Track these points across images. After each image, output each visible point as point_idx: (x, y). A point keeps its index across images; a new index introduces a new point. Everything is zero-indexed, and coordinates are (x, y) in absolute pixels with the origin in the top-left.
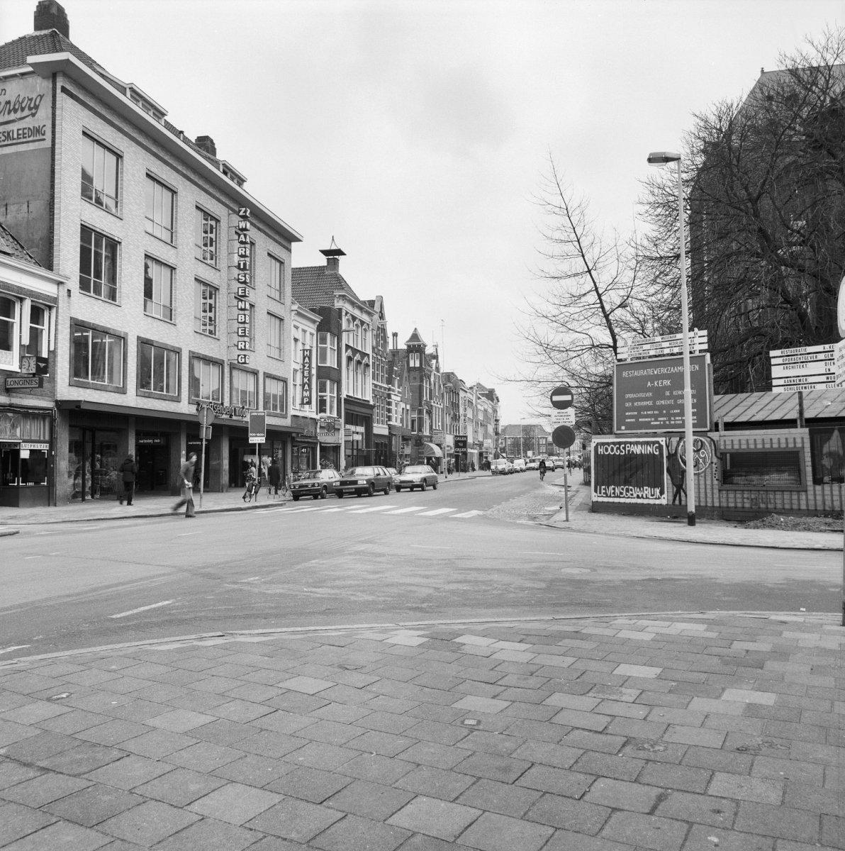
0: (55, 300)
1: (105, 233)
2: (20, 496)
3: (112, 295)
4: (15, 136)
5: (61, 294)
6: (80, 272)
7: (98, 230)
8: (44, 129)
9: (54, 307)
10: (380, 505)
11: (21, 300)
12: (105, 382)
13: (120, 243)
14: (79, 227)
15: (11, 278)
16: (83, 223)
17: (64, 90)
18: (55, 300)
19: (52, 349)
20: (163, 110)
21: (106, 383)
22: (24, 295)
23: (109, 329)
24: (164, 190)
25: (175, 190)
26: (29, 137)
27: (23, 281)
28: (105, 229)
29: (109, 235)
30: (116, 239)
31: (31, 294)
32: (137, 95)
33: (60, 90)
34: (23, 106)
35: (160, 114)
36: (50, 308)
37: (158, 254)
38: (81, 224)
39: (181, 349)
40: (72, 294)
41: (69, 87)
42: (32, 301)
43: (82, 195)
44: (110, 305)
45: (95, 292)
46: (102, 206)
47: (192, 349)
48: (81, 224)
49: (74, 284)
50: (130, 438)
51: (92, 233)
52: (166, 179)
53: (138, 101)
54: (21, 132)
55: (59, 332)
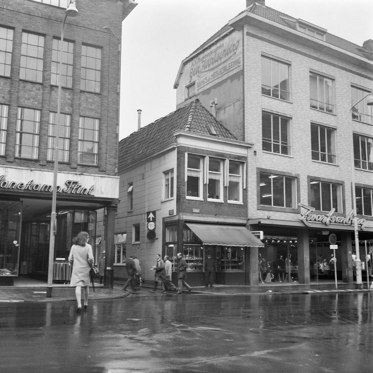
0: (246, 158)
1: (280, 114)
2: (353, 277)
3: (285, 150)
4: (228, 68)
5: (249, 154)
6: (312, 149)
7: (275, 113)
8: (240, 59)
9: (245, 162)
10: (205, 327)
11: (224, 160)
12: (197, 195)
13: (291, 118)
14: (352, 134)
15: (186, 143)
16: (263, 110)
17: (248, 34)
18: (246, 158)
19: (245, 188)
20: (324, 30)
21: (221, 200)
22: (205, 155)
23: (285, 172)
24: (272, 61)
25: (334, 78)
26: (234, 66)
27: (210, 147)
28: (358, 131)
29: (283, 115)
30: (289, 116)
31: (230, 156)
32: (304, 25)
33: (246, 35)
34: (231, 50)
35: (322, 32)
36: (243, 163)
37: (321, 121)
38: (262, 111)
39: (343, 182)
40: (257, 154)
41: (251, 31)
42: (230, 160)
43: (262, 93)
44: (285, 158)
45: (363, 168)
46: (317, 108)
47: (258, 166)
48: (262, 111)
49: (258, 146)
50: (348, 246)
51: (318, 126)
52: (325, 72)
53: (305, 28)
54: (230, 65)
55: (249, 177)
